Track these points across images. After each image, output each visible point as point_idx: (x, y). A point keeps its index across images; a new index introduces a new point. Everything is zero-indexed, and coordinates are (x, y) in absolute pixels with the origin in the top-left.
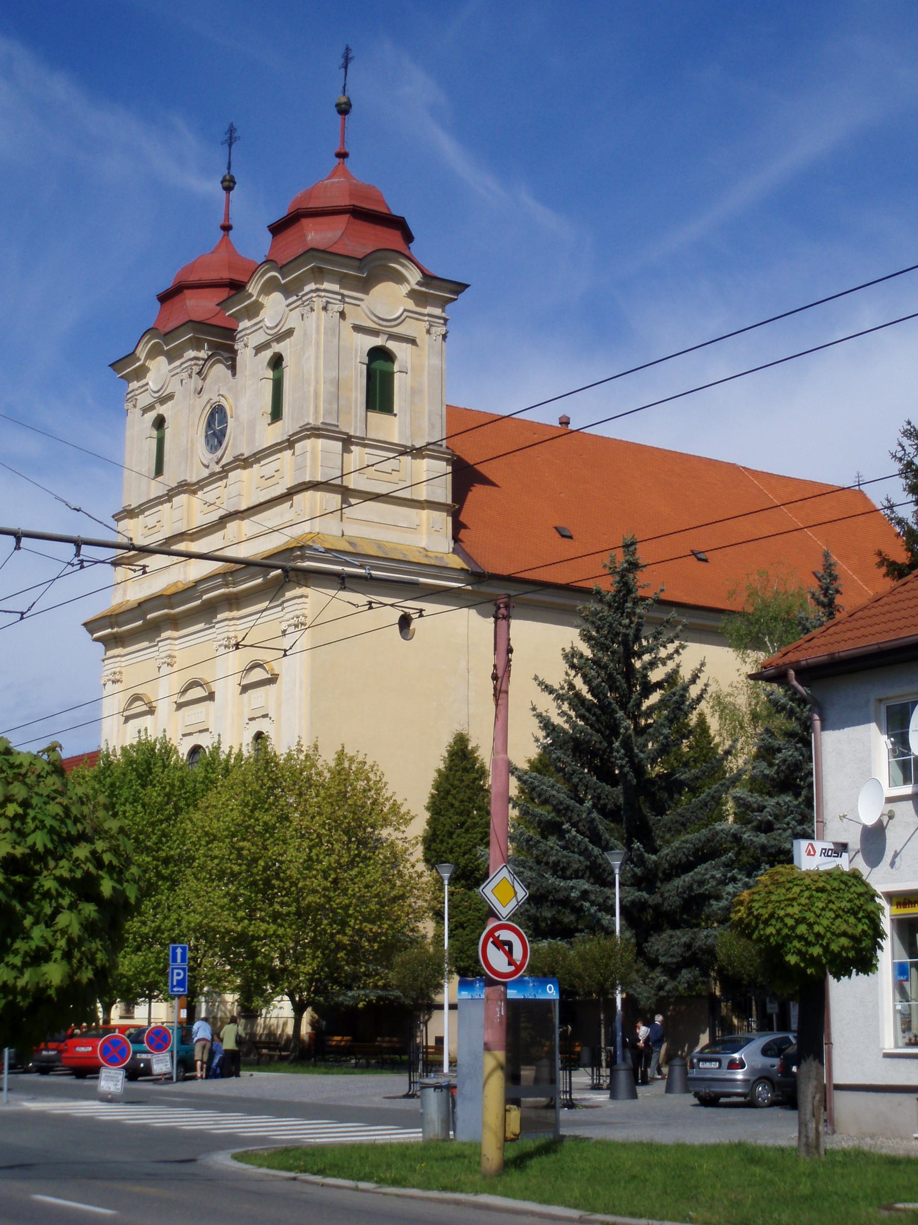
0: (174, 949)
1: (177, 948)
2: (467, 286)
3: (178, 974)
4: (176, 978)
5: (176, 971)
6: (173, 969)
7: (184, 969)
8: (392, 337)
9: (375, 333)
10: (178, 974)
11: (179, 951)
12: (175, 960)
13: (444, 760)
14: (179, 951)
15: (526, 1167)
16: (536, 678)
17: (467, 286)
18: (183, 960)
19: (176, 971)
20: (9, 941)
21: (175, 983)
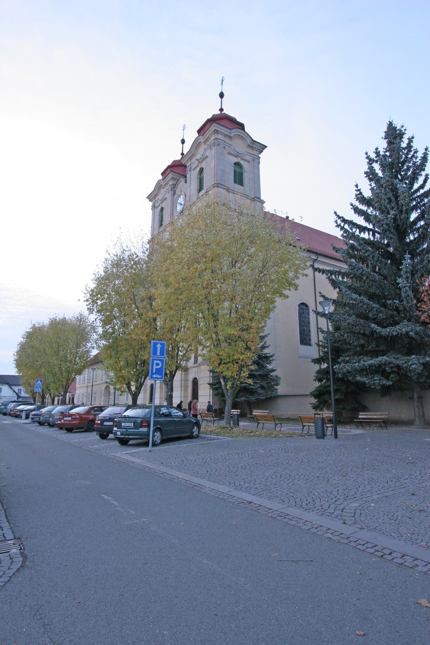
0: (155, 344)
1: (157, 343)
2: (266, 147)
3: (158, 365)
4: (155, 367)
5: (155, 362)
6: (153, 360)
7: (162, 361)
8: (242, 159)
9: (237, 156)
10: (158, 365)
11: (159, 346)
12: (155, 353)
13: (293, 219)
14: (159, 346)
15: (32, 328)
16: (366, 154)
17: (266, 147)
18: (162, 353)
19: (155, 362)
20: (375, 188)
21: (154, 371)
